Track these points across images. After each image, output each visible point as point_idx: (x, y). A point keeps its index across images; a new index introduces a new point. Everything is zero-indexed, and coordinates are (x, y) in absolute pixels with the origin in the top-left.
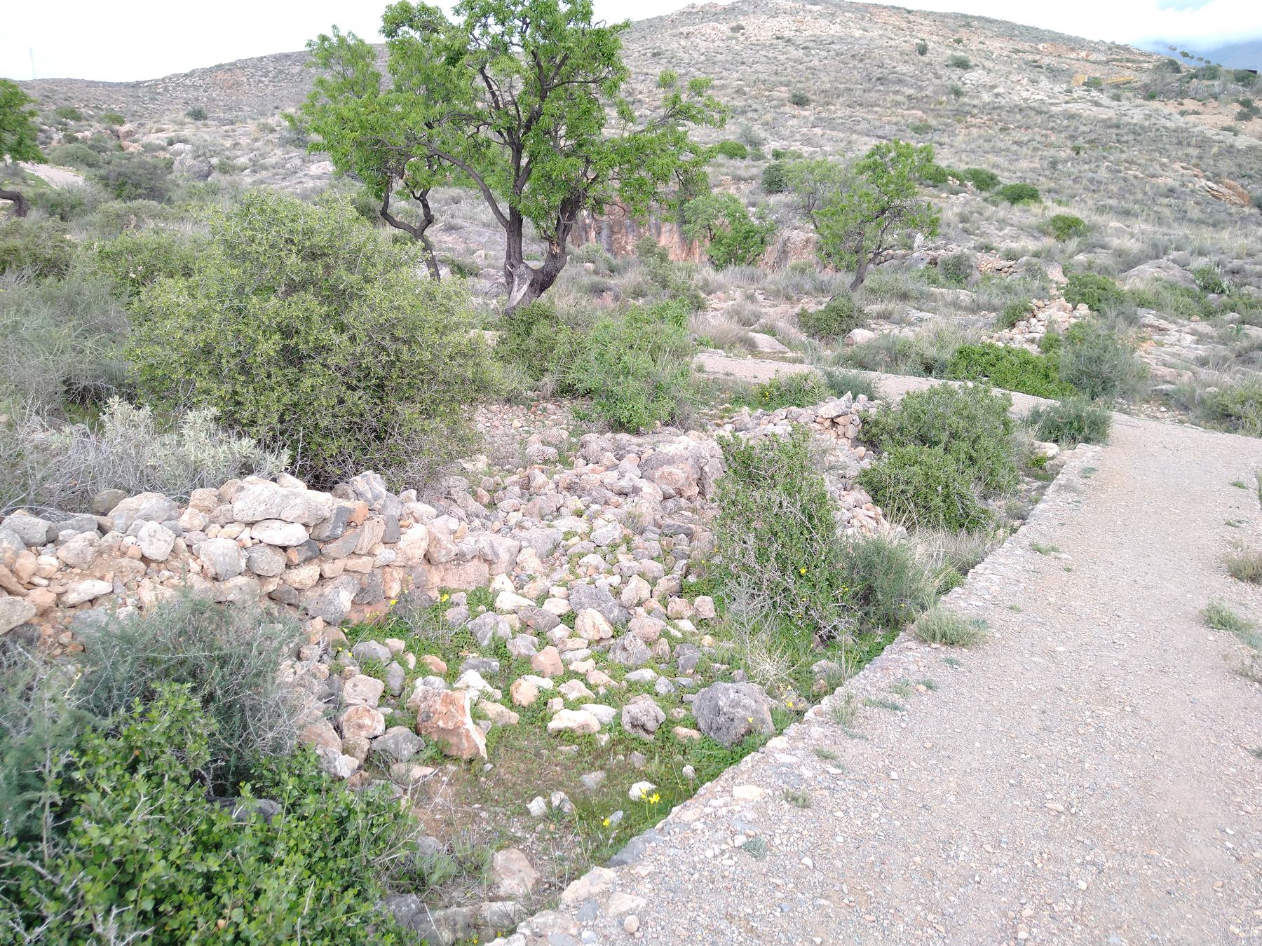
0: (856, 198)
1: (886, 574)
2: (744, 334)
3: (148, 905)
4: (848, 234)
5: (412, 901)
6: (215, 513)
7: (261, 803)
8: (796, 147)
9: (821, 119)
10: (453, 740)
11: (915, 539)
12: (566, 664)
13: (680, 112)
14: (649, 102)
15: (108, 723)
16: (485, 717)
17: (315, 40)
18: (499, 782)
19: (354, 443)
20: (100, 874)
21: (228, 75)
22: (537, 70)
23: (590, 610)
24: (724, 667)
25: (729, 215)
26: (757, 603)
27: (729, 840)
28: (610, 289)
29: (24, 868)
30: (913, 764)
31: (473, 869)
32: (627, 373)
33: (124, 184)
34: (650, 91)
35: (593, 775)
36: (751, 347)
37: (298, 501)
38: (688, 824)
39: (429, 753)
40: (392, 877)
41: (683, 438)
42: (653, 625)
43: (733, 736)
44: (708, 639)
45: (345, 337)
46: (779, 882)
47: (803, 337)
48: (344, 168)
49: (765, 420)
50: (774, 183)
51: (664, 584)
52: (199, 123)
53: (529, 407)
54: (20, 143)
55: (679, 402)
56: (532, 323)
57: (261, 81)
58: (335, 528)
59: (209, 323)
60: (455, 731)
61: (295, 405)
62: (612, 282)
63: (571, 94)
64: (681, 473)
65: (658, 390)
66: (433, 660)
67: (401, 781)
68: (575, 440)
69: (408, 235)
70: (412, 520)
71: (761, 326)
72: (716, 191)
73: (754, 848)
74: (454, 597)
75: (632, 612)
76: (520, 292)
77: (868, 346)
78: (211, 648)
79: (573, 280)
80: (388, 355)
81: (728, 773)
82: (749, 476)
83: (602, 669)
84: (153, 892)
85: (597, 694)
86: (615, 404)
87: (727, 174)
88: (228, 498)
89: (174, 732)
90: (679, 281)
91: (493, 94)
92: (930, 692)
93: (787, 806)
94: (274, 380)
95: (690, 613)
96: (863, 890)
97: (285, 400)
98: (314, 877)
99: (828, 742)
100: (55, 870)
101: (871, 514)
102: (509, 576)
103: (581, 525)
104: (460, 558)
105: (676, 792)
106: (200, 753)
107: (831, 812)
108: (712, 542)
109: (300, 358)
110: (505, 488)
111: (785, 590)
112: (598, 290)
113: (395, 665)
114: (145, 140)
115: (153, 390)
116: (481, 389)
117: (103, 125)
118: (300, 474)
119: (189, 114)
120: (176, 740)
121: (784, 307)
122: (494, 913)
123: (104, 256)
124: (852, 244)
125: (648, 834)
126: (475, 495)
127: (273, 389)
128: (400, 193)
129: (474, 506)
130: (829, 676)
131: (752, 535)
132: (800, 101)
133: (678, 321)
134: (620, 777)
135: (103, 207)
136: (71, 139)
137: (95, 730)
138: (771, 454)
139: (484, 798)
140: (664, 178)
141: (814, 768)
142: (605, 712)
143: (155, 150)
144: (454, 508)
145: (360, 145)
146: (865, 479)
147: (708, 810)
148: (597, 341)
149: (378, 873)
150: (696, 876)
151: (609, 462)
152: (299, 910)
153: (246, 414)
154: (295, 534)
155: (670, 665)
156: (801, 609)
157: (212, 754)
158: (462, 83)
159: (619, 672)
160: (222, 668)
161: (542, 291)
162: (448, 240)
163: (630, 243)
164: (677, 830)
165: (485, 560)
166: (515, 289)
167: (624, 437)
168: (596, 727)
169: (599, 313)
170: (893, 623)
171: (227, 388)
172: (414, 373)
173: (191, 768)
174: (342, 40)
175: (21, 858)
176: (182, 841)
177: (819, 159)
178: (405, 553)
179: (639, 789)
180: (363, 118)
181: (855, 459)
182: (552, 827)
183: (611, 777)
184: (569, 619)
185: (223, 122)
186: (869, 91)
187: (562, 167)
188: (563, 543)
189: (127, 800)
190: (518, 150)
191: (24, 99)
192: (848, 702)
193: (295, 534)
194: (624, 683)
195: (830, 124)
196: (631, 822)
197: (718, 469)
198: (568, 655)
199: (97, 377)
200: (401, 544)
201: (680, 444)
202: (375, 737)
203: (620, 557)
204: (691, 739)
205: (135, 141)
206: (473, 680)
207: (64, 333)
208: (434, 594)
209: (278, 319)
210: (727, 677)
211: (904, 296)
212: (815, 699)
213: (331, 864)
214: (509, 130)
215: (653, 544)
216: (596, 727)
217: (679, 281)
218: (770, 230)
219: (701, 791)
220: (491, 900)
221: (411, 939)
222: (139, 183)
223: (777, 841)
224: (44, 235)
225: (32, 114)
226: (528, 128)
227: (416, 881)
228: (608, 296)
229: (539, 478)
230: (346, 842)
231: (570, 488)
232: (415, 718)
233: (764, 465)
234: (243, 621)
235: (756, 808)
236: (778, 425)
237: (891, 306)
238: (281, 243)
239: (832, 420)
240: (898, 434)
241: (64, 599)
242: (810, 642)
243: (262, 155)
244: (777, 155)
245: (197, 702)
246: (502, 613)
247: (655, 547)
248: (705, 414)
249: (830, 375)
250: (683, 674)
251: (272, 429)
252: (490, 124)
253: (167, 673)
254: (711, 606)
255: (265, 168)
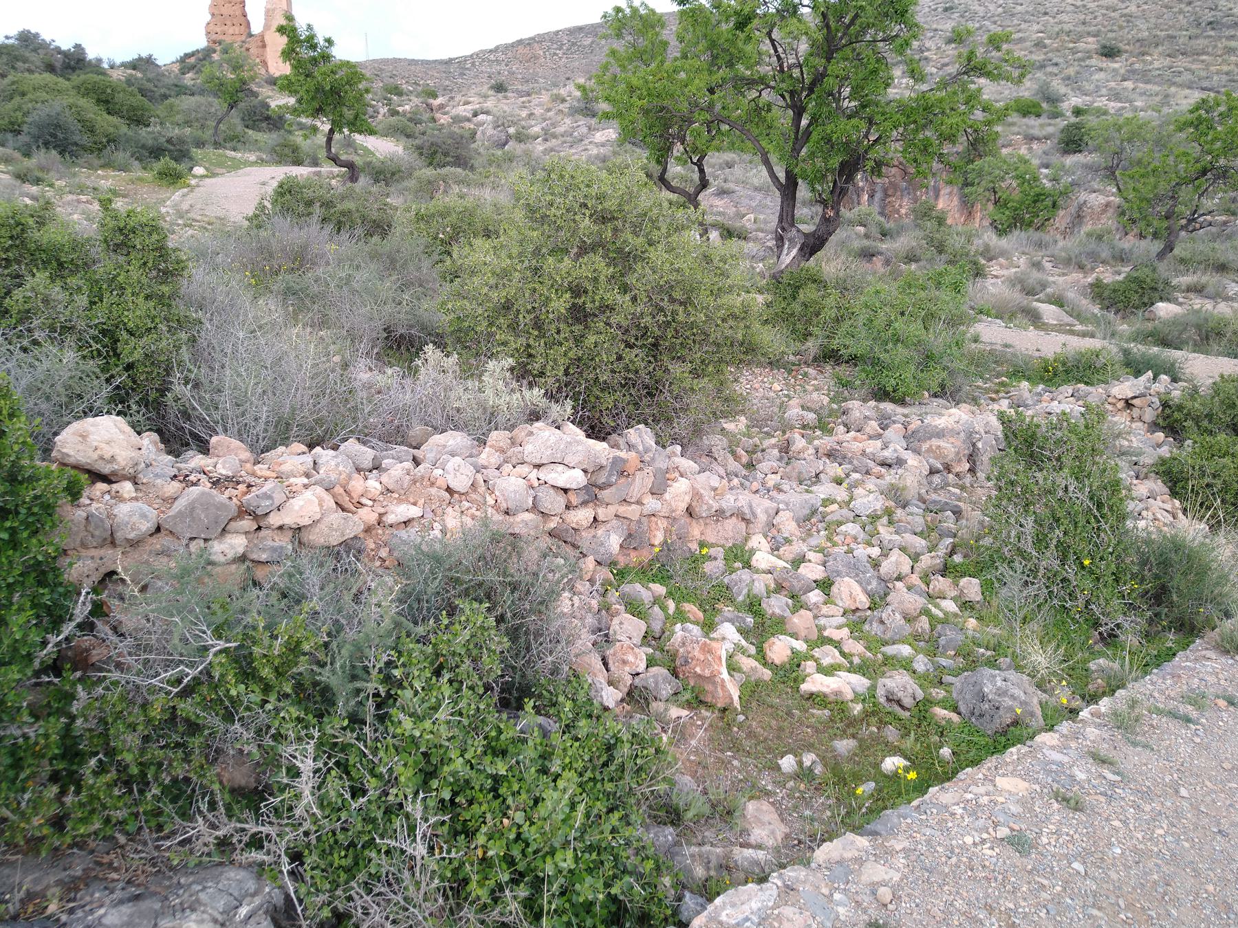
0: (1172, 158)
1: (1185, 574)
2: (1029, 307)
3: (447, 795)
4: (1159, 199)
5: (669, 833)
6: (509, 454)
7: (540, 719)
8: (1101, 102)
9: (1134, 72)
10: (709, 687)
11: (1221, 539)
12: (821, 629)
13: (974, 68)
14: (938, 56)
15: (420, 630)
16: (739, 670)
17: (610, 11)
18: (751, 734)
19: (628, 398)
20: (411, 761)
21: (526, 50)
22: (825, 30)
23: (847, 579)
24: (989, 653)
25: (1017, 177)
26: (1032, 590)
27: (991, 830)
28: (881, 254)
29: (352, 745)
30: (1209, 784)
31: (725, 813)
32: (897, 340)
33: (435, 152)
34: (939, 48)
35: (845, 742)
36: (1035, 318)
37: (580, 448)
38: (946, 807)
39: (688, 696)
40: (650, 807)
41: (953, 410)
42: (915, 602)
43: (997, 724)
44: (972, 623)
45: (627, 297)
46: (1045, 882)
47: (1096, 310)
48: (628, 136)
49: (1047, 396)
50: (1072, 142)
51: (926, 561)
52: (500, 95)
53: (790, 372)
54: (356, 117)
55: (951, 373)
56: (799, 287)
57: (555, 54)
58: (610, 475)
59: (510, 281)
60: (711, 679)
61: (579, 359)
62: (884, 246)
63: (858, 54)
64: (949, 447)
65: (928, 359)
66: (691, 608)
67: (660, 718)
68: (835, 406)
69: (682, 199)
70: (677, 474)
71: (1047, 295)
72: (1004, 151)
73: (1018, 843)
74: (713, 551)
75: (890, 585)
76: (789, 255)
77: (1174, 321)
78: (505, 575)
79: (843, 243)
80: (665, 316)
81: (991, 762)
82: (1031, 456)
83: (858, 639)
84: (451, 784)
85: (851, 663)
86: (881, 373)
87: (1018, 134)
88: (519, 441)
89: (471, 646)
90: (958, 246)
91: (779, 58)
92: (1231, 709)
93: (1056, 805)
94: (562, 335)
95: (954, 593)
96: (1143, 908)
97: (571, 354)
98: (584, 795)
99: (1106, 746)
100: (375, 751)
101: (1168, 507)
102: (766, 536)
103: (841, 494)
104: (720, 514)
105: (934, 773)
106: (493, 666)
107: (1107, 820)
108: (981, 523)
109: (585, 316)
110: (763, 451)
111: (1064, 580)
112: (868, 255)
113: (656, 608)
114: (454, 112)
115: (459, 340)
116: (748, 353)
117: (420, 100)
118: (580, 424)
119: (492, 88)
120: (474, 651)
121: (1076, 276)
122: (747, 859)
123: (420, 218)
124: (1162, 210)
125: (903, 809)
126: (733, 453)
127: (561, 344)
128: (678, 159)
129: (733, 465)
130: (1110, 678)
131: (1031, 519)
132: (1109, 52)
133: (956, 288)
134: (873, 748)
135: (417, 173)
136: (394, 113)
137: (408, 636)
138: (1059, 434)
139: (736, 747)
140: (951, 138)
141: (1089, 771)
142: (860, 682)
143: (461, 121)
144: (714, 465)
145: (646, 112)
146: (1163, 468)
147: (969, 796)
148: (867, 306)
149: (639, 800)
150: (954, 860)
151: (871, 431)
152: (572, 822)
153: (537, 366)
154: (575, 478)
155: (932, 646)
156: (1081, 603)
157: (502, 670)
158: (749, 48)
159: (874, 643)
160: (513, 592)
161: (811, 255)
162: (720, 204)
163: (904, 206)
164: (935, 811)
165: (743, 519)
166: (785, 252)
167: (888, 406)
168: (849, 695)
169: (869, 278)
170: (1189, 629)
171: (522, 341)
172: (688, 333)
173: (485, 680)
174: (635, 11)
175: (350, 737)
176: (476, 743)
177: (1129, 115)
178: (670, 504)
179: (892, 763)
180: (651, 86)
181: (1151, 446)
182: (802, 786)
183: (863, 746)
184: (825, 585)
185: (520, 94)
186: (1197, 37)
187: (844, 129)
188: (821, 509)
189: (434, 700)
190: (799, 112)
191: (362, 77)
192: (1132, 707)
193: (575, 478)
194: (880, 656)
195: (1145, 76)
196: (884, 794)
197: (992, 446)
198: (822, 621)
199: (411, 326)
200: (667, 496)
201: (952, 417)
202: (638, 674)
203: (881, 529)
204: (949, 721)
205: (445, 114)
206: (728, 632)
207: (388, 286)
208: (694, 546)
209: (570, 279)
210: (992, 663)
211: (1222, 268)
212: (1093, 699)
213: (599, 785)
214: (792, 93)
215: (915, 517)
216: (849, 695)
217: (958, 246)
218: (1064, 194)
219: (961, 775)
220: (742, 846)
221: (668, 868)
222: (446, 152)
223: (1045, 840)
224: (371, 199)
225: (367, 91)
226: (811, 91)
227: (671, 815)
228: (878, 261)
229: (799, 443)
230: (613, 768)
231: (830, 455)
232: (674, 661)
233: (1050, 445)
234: (531, 554)
235: (1022, 802)
236: (1063, 403)
237: (1204, 279)
238: (576, 206)
239: (1127, 401)
240: (1205, 421)
241: (384, 519)
242: (1088, 638)
243: (552, 124)
244: (1078, 112)
245: (492, 621)
246: (757, 571)
247: (919, 522)
248: (978, 387)
249: (1126, 352)
250: (943, 655)
251: (558, 381)
252: (773, 88)
253: (466, 593)
254: (977, 589)
255: (555, 136)
